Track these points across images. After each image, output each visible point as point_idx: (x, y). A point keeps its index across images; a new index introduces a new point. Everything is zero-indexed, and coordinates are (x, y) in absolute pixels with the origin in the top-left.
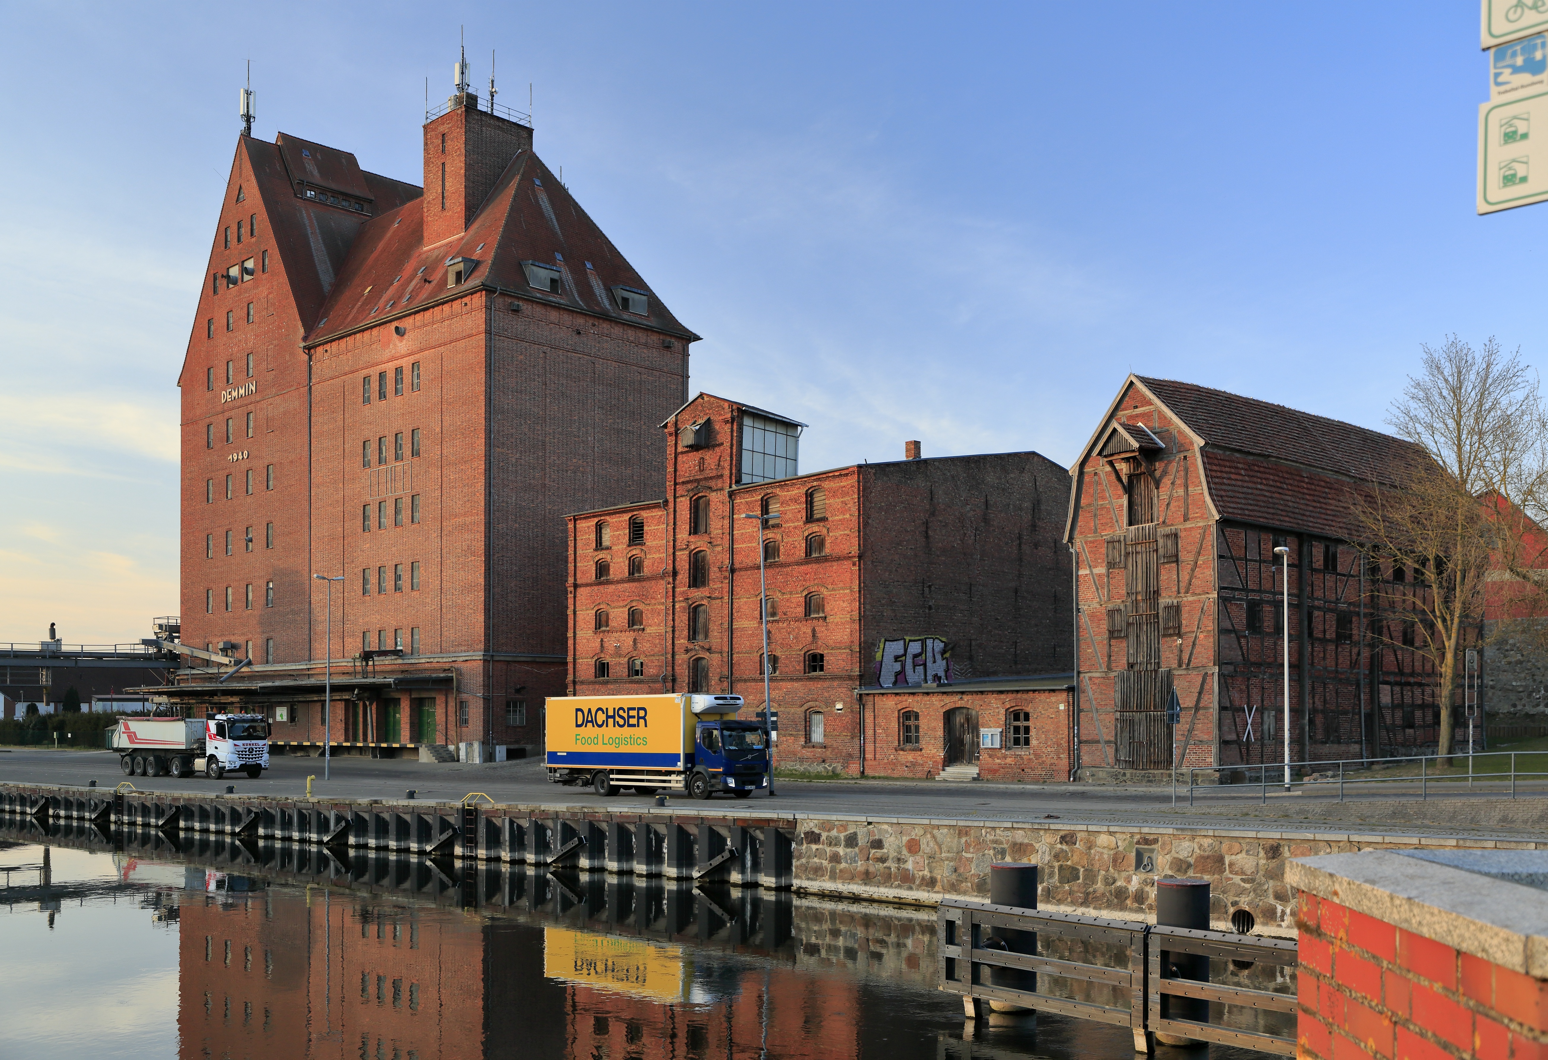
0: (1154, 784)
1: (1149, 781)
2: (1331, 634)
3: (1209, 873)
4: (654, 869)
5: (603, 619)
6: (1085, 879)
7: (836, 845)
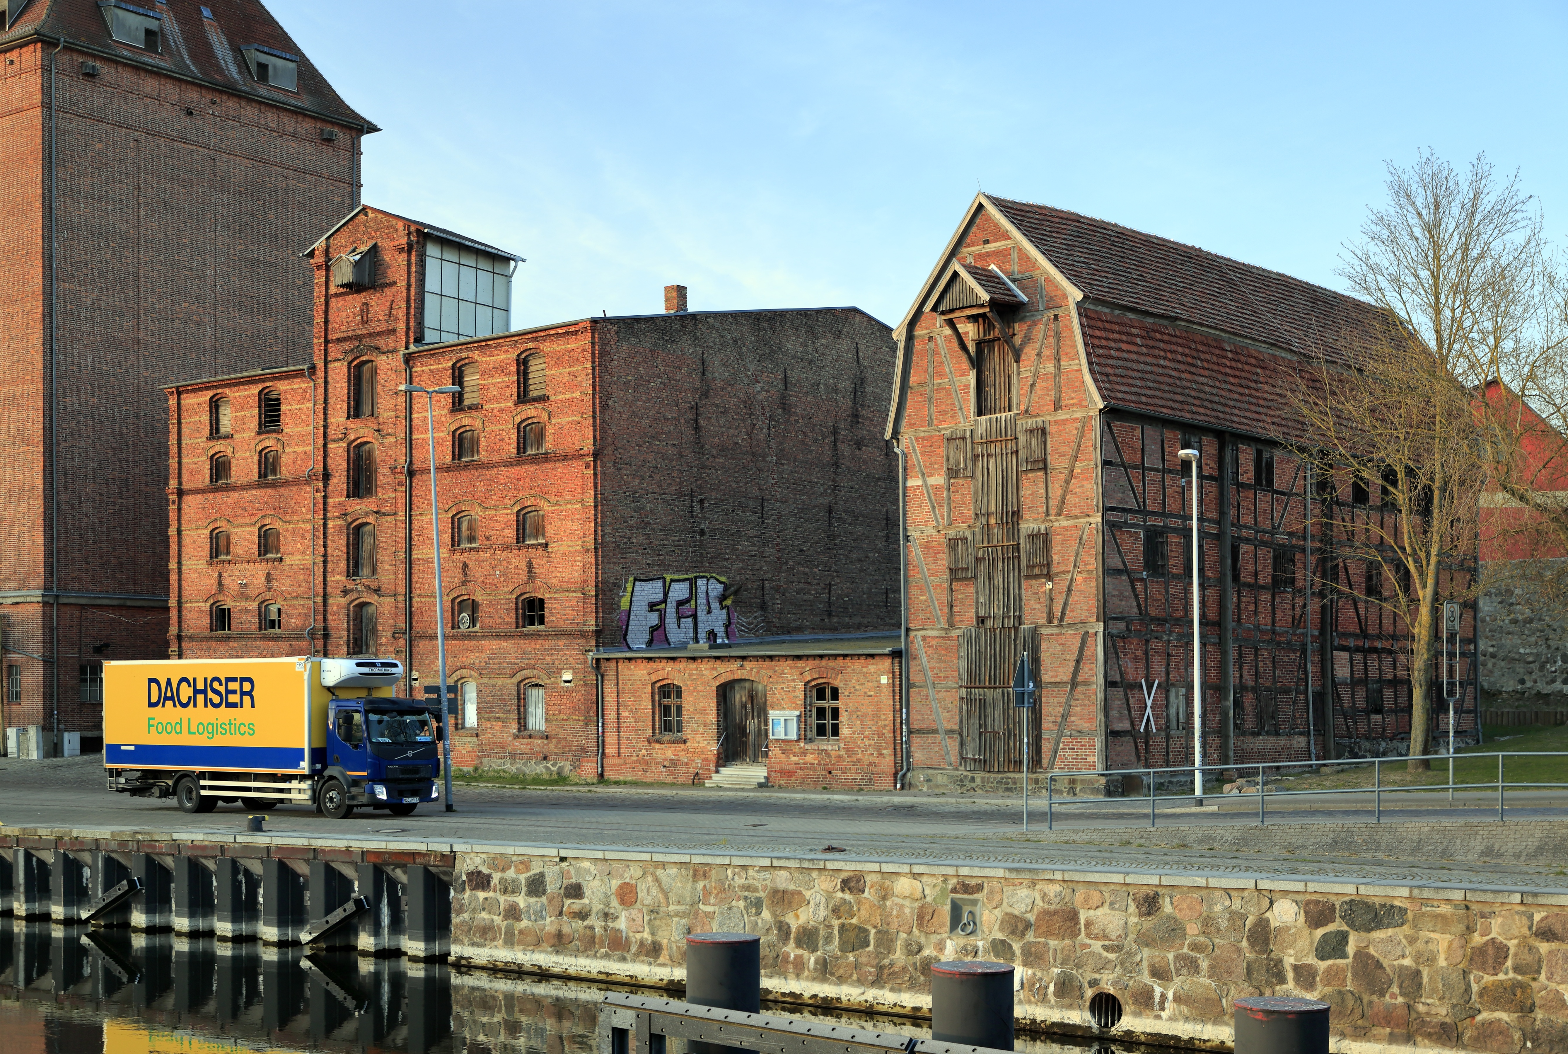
0: (1014, 795)
1: (1008, 789)
2: (1265, 578)
3: (1057, 936)
4: (244, 928)
5: (222, 542)
6: (877, 946)
7: (513, 892)
